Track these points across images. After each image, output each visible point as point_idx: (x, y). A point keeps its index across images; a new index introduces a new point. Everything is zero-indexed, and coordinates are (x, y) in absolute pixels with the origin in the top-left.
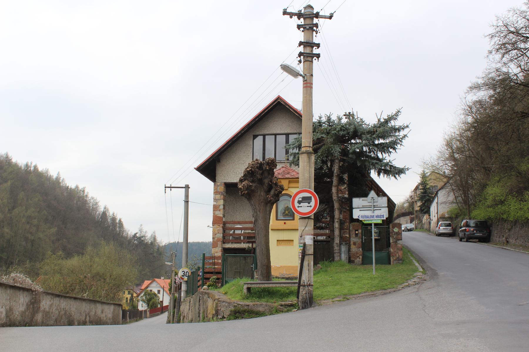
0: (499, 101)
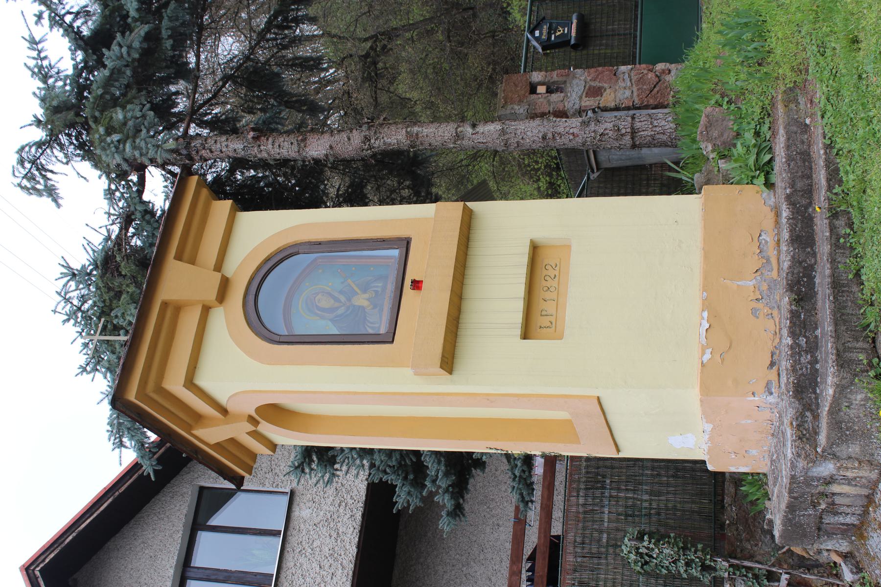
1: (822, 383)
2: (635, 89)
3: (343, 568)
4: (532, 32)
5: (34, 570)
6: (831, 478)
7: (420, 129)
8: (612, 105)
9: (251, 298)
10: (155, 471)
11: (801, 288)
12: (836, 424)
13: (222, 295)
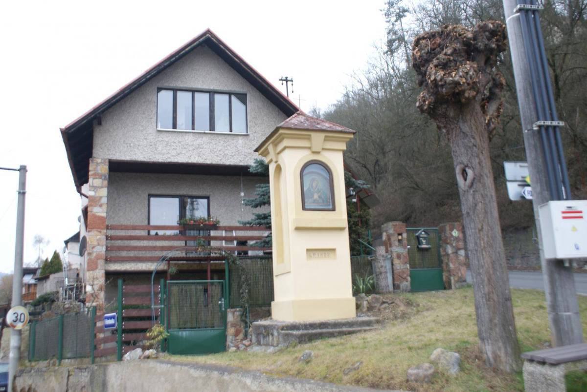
0: (336, 112)
2: (400, 270)
3: (220, 160)
4: (424, 231)
8: (394, 263)
9: (314, 162)
12: (287, 335)
13: (314, 153)
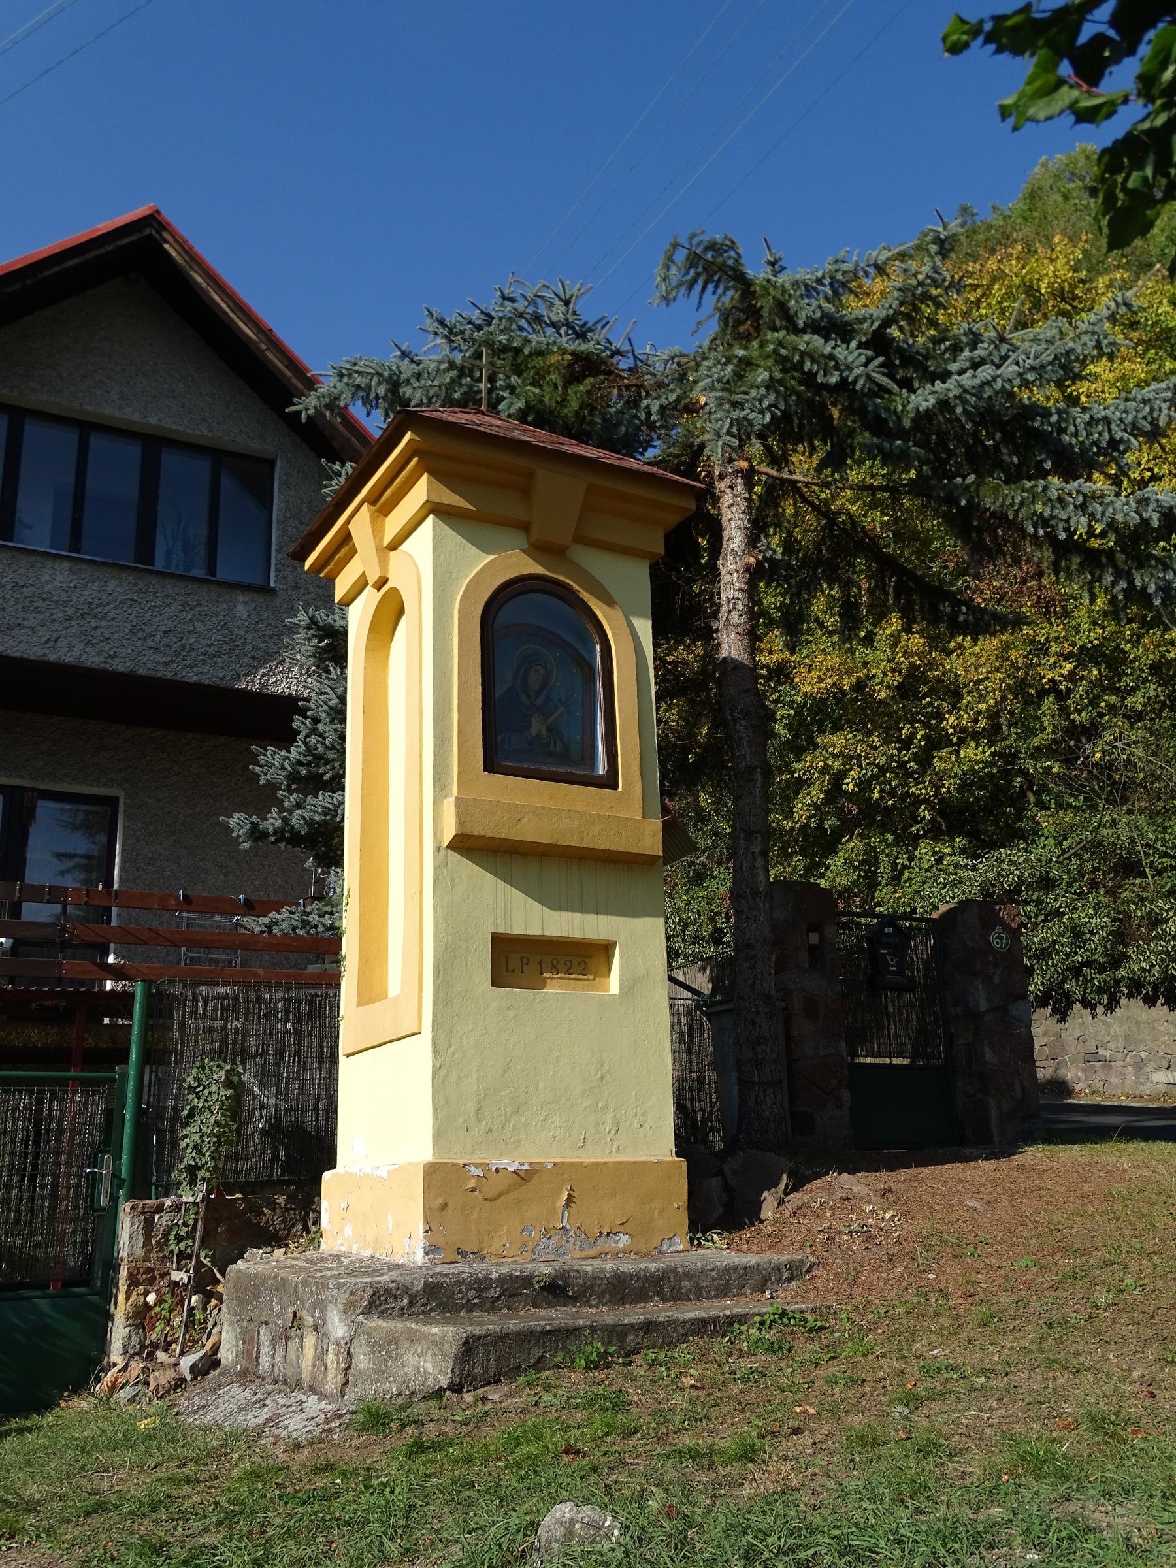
1: (444, 1318)
3: (166, 664)
5: (153, 227)
6: (324, 1334)
7: (759, 785)
10: (299, 413)
11: (557, 1289)
